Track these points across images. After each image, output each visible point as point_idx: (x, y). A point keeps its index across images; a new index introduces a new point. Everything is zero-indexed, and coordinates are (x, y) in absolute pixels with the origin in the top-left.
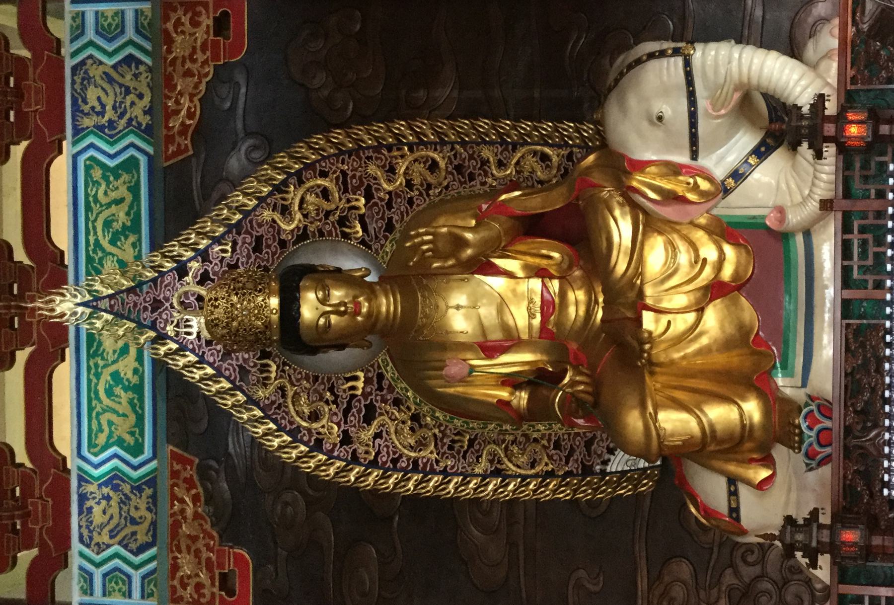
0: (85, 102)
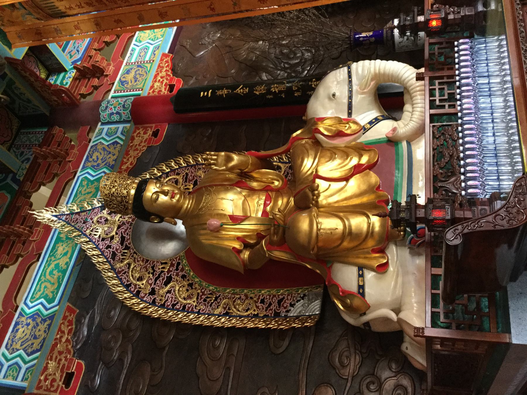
0: (91, 157)
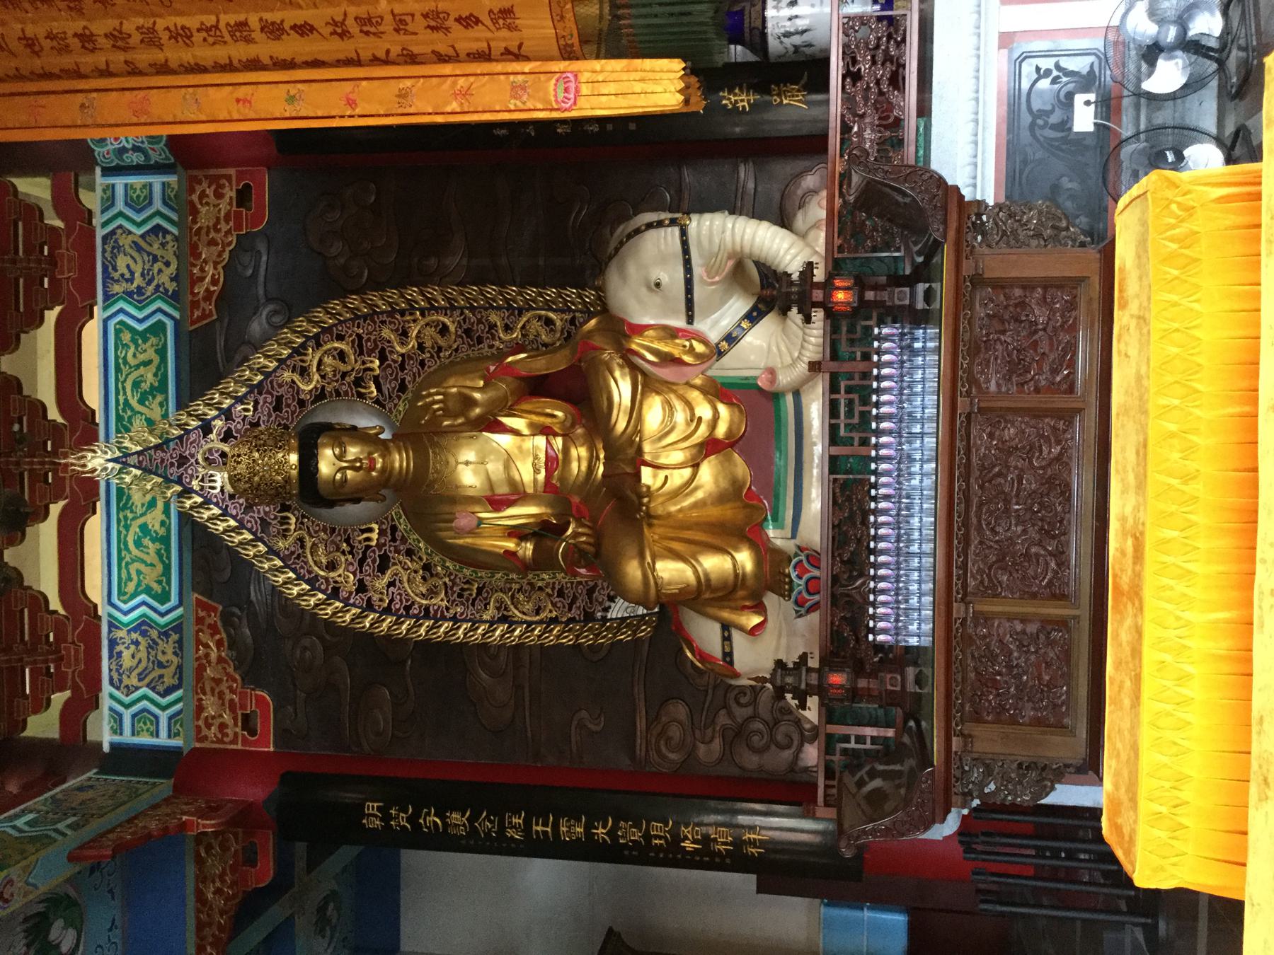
0: (115, 269)
